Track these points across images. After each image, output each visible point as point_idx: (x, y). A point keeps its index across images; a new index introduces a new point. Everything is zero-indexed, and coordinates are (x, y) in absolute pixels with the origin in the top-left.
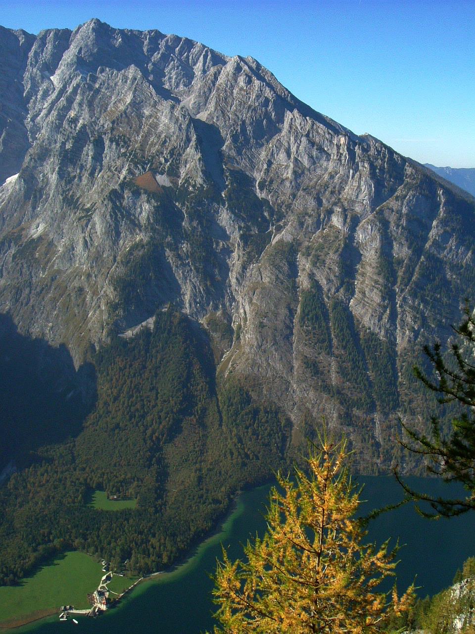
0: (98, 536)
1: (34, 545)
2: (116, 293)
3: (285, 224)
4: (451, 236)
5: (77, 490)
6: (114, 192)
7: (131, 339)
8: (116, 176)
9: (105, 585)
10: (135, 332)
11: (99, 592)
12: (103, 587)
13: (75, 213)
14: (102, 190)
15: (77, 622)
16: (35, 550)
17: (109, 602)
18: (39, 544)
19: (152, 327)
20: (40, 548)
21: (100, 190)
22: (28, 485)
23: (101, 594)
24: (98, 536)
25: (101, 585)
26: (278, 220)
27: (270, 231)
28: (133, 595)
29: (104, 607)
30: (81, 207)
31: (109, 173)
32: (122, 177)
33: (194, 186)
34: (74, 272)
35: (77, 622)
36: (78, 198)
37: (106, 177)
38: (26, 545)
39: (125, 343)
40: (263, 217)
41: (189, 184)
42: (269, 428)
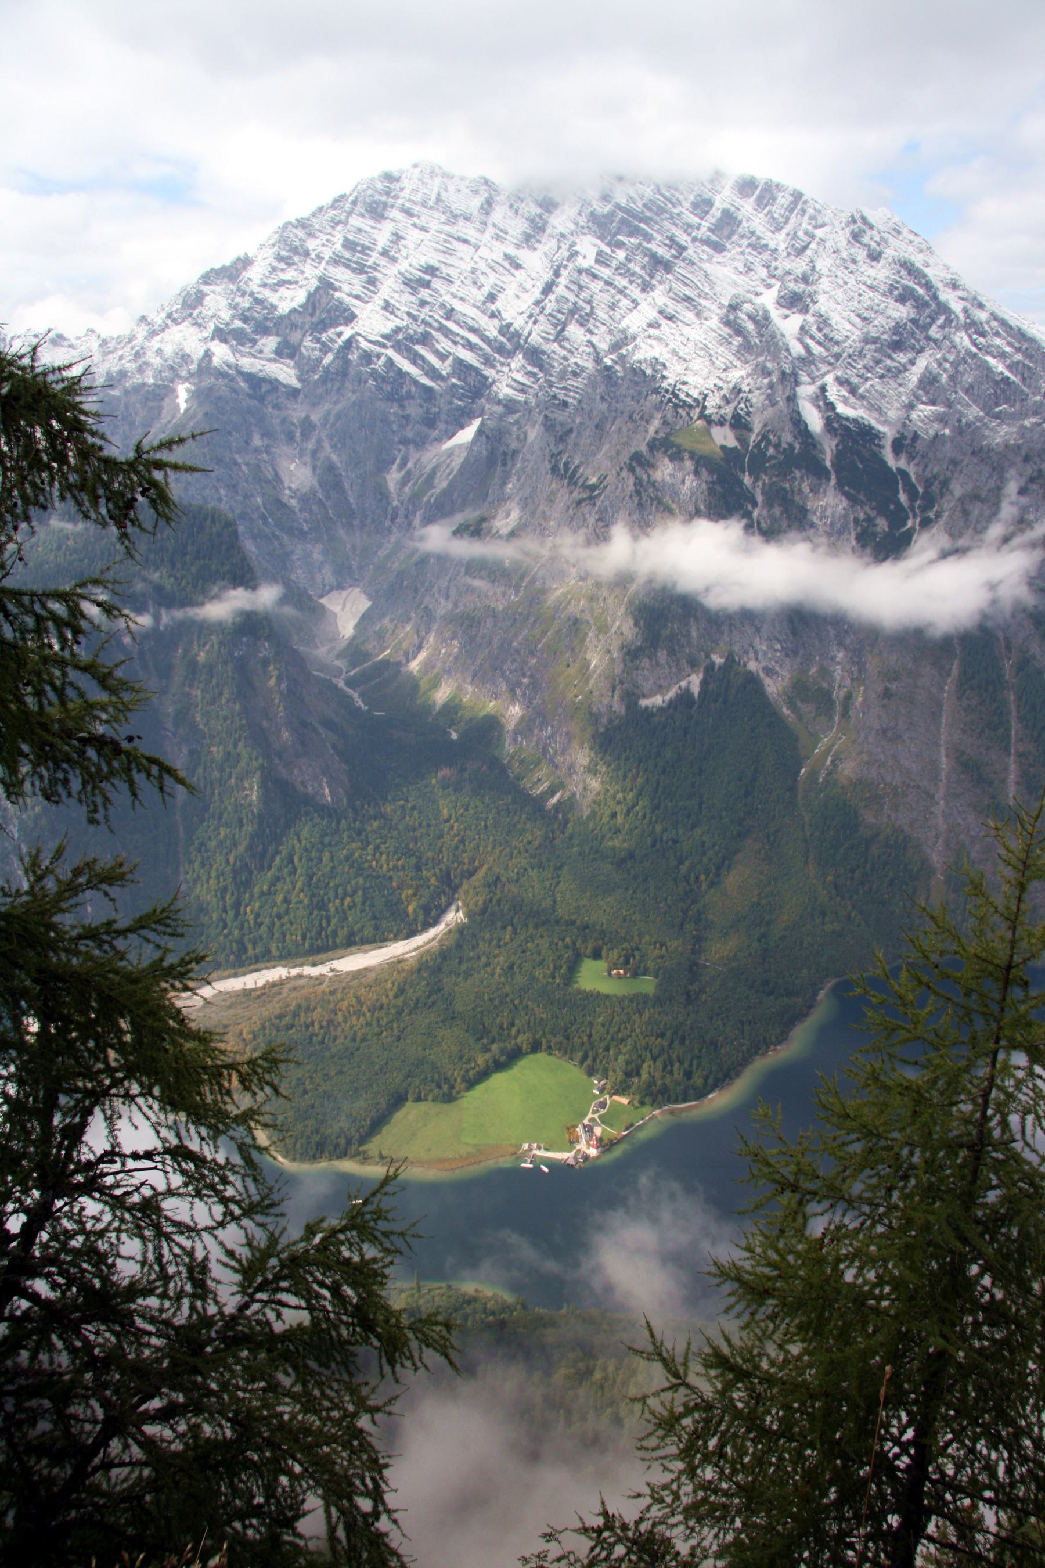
0: (590, 1036)
1: (485, 1041)
2: (637, 630)
3: (938, 515)
4: (588, 817)
5: (560, 957)
6: (637, 457)
7: (661, 709)
8: (641, 429)
9: (596, 1116)
10: (667, 697)
11: (585, 1127)
12: (592, 1120)
13: (571, 493)
14: (618, 453)
15: (546, 1170)
16: (486, 1049)
17: (606, 1145)
18: (493, 1042)
19: (696, 690)
20: (495, 1047)
21: (614, 453)
22: (481, 943)
23: (589, 1130)
24: (590, 1036)
25: (590, 1116)
26: (924, 509)
27: (909, 530)
28: (642, 1136)
29: (593, 1152)
30: (581, 481)
31: (630, 425)
32: (652, 430)
33: (777, 446)
34: (568, 592)
35: (546, 1170)
36: (578, 467)
37: (624, 429)
38: (471, 1041)
39: (648, 714)
40: (898, 503)
41: (769, 443)
42: (891, 874)
